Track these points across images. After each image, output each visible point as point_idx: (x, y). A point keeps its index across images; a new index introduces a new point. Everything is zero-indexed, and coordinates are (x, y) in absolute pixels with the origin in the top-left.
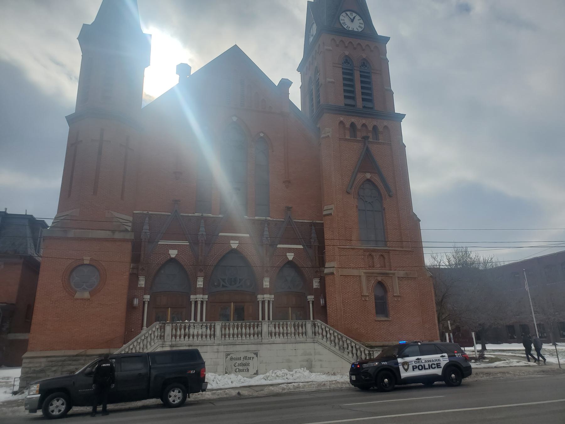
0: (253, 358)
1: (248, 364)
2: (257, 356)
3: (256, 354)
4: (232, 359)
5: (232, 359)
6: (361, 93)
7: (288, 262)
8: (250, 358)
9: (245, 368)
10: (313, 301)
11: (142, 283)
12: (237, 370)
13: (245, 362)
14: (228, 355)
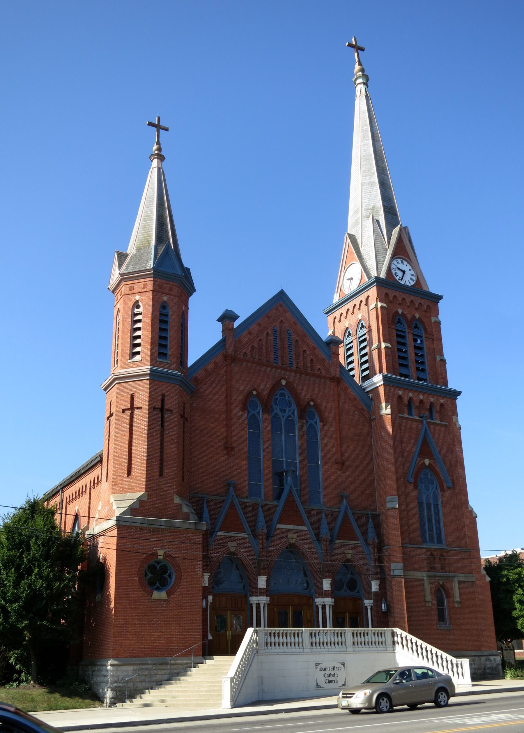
0: (341, 668)
1: (337, 676)
2: (344, 666)
3: (343, 664)
4: (321, 669)
5: (321, 669)
6: (415, 361)
7: (347, 560)
8: (338, 669)
9: (334, 679)
10: (371, 607)
12: (327, 681)
13: (333, 673)
14: (317, 665)
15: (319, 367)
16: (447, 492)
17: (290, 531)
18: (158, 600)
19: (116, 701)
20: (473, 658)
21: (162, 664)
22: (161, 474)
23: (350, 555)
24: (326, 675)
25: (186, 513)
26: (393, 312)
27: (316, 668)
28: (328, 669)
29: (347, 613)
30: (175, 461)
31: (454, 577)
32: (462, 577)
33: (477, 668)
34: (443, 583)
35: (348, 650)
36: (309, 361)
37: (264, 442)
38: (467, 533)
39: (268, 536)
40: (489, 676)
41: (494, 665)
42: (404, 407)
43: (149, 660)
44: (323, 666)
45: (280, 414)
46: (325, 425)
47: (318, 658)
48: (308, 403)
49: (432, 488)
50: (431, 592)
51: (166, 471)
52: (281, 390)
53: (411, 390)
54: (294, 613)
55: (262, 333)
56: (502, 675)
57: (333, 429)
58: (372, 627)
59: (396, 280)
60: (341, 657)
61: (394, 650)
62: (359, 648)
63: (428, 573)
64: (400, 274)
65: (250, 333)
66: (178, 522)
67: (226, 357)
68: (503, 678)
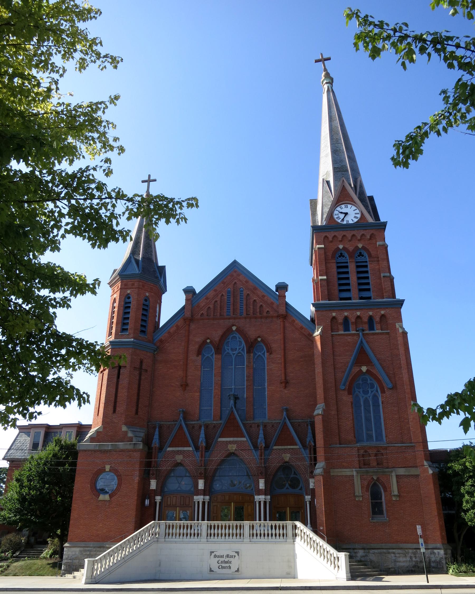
1: (231, 562)
2: (238, 555)
3: (238, 553)
4: (215, 556)
5: (215, 556)
8: (232, 557)
9: (227, 565)
11: (153, 484)
12: (220, 567)
13: (227, 560)
14: (212, 552)
15: (268, 309)
16: (388, 393)
17: (230, 442)
18: (103, 500)
19: (66, 572)
20: (415, 550)
21: (100, 547)
22: (114, 411)
23: (288, 458)
24: (220, 562)
25: (130, 437)
26: (333, 249)
27: (211, 555)
28: (222, 557)
29: (288, 508)
30: (125, 401)
31: (392, 472)
32: (401, 471)
33: (419, 561)
34: (378, 478)
35: (245, 540)
36: (258, 307)
37: (215, 376)
38: (411, 429)
39: (207, 448)
40: (434, 569)
41: (438, 559)
42: (339, 326)
43: (91, 544)
44: (217, 554)
45: (231, 352)
46: (271, 354)
47: (213, 547)
48: (256, 339)
49: (372, 392)
50: (362, 487)
51: (118, 409)
52: (233, 334)
53: (333, 310)
54: (236, 509)
55: (218, 296)
56: (445, 569)
57: (279, 356)
58: (208, 520)
59: (338, 223)
60: (236, 547)
61: (294, 542)
62: (170, 539)
63: (359, 469)
64: (342, 216)
65: (207, 299)
66: (121, 445)
67: (185, 320)
68: (447, 573)
